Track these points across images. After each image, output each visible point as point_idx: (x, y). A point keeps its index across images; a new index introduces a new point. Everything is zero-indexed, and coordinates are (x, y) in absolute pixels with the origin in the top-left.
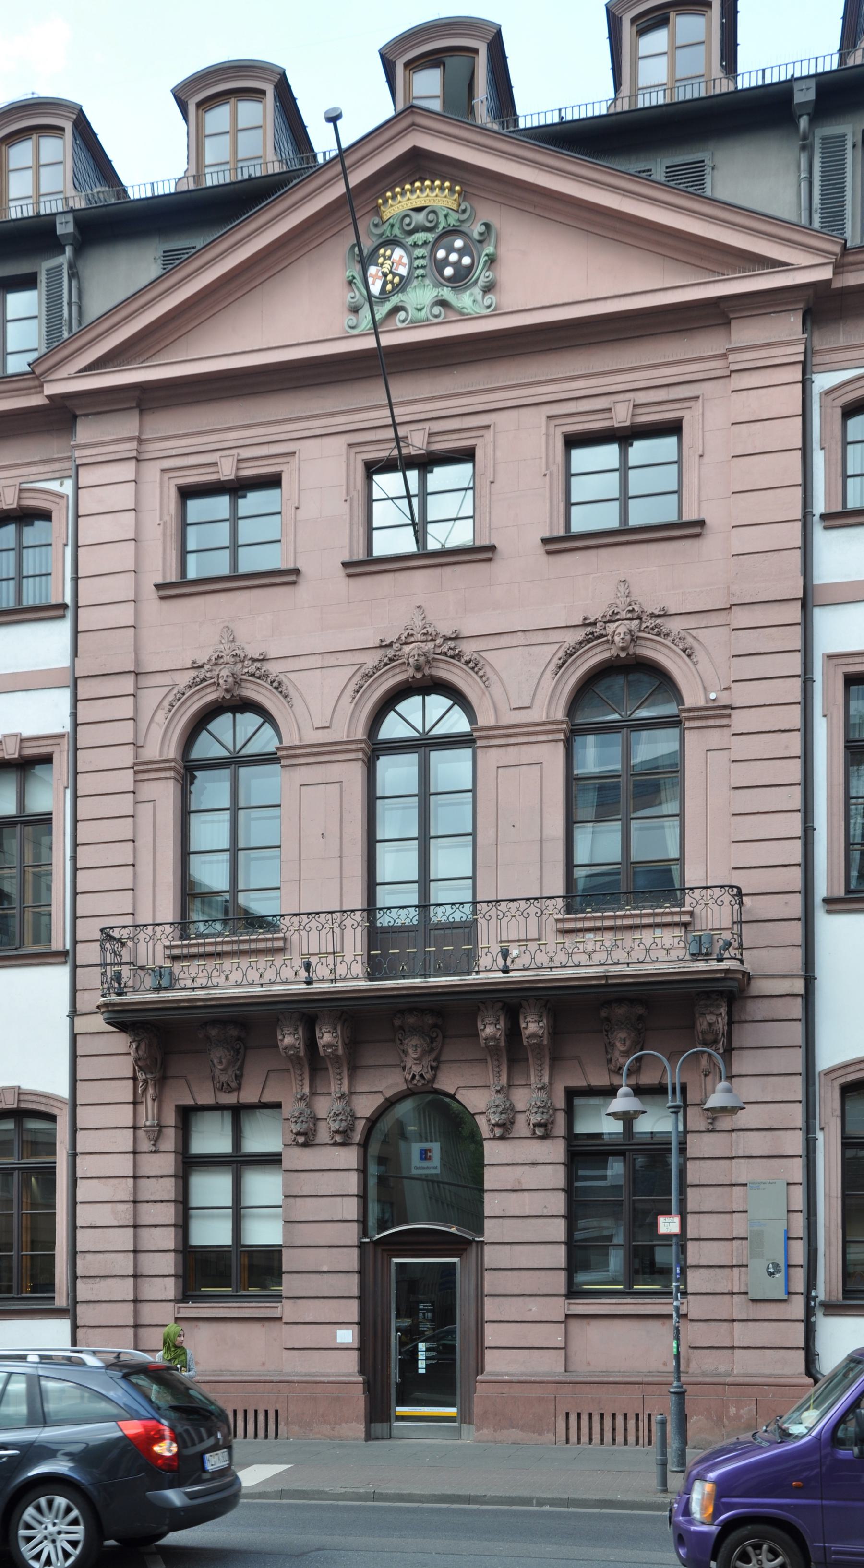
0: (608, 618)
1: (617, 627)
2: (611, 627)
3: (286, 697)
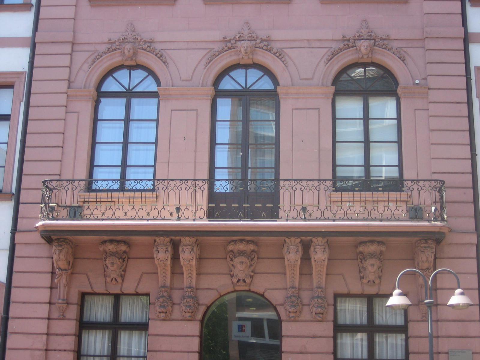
0: (357, 37)
1: (362, 43)
2: (239, 44)
3: (164, 63)
